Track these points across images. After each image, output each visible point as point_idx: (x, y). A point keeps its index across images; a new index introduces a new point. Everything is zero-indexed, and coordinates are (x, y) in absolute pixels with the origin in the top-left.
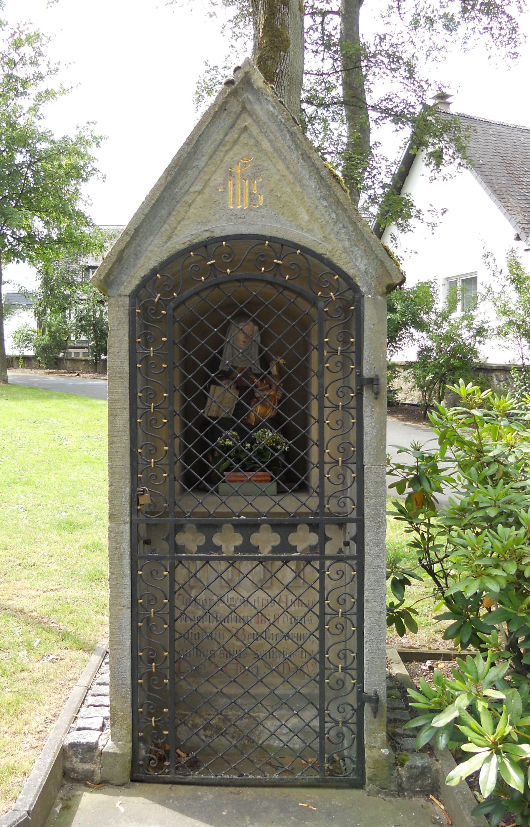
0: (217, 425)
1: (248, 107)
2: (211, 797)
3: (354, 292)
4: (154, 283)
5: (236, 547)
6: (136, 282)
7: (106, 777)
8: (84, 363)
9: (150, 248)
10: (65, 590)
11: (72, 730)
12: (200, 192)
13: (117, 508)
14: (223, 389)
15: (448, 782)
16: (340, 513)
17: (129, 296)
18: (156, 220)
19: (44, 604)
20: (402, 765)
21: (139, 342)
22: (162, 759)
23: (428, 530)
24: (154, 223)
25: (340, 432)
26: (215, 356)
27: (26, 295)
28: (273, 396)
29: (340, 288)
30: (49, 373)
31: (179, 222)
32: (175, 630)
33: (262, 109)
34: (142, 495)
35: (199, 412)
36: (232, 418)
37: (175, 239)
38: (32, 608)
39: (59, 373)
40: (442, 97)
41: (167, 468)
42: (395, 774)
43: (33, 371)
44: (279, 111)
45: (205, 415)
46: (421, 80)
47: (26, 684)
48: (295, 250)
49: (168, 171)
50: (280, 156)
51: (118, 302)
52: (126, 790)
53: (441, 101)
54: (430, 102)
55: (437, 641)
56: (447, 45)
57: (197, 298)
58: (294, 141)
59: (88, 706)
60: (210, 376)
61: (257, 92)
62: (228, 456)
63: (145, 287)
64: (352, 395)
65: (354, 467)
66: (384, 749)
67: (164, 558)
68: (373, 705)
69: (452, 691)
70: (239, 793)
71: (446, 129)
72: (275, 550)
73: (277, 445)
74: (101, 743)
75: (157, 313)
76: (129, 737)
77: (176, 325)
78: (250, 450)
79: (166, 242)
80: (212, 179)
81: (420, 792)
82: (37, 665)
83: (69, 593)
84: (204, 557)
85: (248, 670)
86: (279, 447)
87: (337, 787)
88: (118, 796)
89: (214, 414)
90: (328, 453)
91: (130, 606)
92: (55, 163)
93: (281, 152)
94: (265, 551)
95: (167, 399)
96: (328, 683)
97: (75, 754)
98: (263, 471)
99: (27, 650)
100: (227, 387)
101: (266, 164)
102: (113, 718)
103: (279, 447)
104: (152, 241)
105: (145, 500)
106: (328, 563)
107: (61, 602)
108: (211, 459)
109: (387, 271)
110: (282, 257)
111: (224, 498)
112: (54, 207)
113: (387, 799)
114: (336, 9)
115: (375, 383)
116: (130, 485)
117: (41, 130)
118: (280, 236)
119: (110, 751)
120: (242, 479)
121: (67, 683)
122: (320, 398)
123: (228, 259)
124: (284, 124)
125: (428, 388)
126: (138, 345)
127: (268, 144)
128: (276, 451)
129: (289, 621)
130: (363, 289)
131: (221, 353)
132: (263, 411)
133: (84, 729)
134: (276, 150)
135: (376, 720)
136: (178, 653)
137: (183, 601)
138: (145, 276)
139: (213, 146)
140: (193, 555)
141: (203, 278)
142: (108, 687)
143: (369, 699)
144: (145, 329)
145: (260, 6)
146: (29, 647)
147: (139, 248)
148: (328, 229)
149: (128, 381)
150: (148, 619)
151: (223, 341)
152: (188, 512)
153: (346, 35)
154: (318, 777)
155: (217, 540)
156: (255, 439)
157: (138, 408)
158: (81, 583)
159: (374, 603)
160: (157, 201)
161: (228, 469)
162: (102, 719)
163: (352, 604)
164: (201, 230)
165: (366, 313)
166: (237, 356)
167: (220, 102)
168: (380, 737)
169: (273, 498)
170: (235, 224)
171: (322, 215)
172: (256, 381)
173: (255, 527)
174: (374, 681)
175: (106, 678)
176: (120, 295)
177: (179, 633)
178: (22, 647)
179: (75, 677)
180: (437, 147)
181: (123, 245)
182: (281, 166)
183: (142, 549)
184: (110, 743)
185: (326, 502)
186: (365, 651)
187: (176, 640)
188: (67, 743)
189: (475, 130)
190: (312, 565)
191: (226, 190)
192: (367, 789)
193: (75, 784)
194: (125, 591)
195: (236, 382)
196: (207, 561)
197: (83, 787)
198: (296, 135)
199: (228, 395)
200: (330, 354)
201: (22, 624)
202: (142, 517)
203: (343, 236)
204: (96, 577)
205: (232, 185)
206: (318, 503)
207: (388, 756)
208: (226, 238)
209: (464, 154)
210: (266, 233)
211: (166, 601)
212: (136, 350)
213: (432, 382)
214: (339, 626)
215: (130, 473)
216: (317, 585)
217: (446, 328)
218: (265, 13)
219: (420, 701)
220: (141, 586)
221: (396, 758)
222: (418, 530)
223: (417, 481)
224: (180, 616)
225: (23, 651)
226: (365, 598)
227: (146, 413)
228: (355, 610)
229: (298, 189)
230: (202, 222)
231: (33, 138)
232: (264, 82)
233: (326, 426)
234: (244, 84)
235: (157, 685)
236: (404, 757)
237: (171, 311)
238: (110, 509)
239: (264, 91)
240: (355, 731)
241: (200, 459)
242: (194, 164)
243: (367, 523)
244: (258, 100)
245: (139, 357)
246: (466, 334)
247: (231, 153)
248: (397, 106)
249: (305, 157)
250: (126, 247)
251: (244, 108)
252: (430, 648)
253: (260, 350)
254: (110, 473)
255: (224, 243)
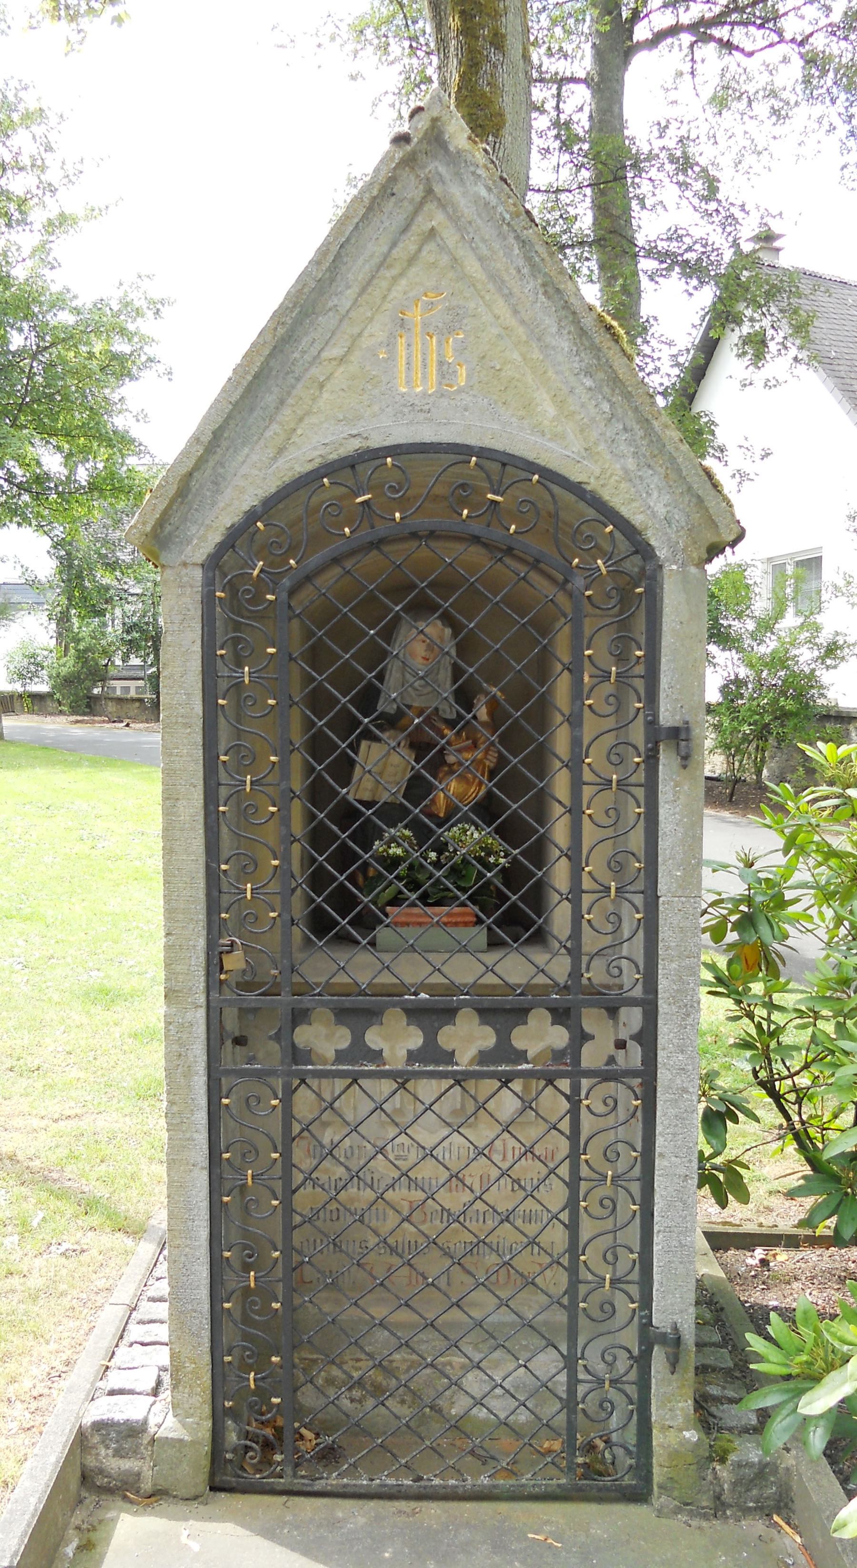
0: (374, 818)
1: (438, 189)
2: (361, 1520)
3: (644, 559)
4: (252, 540)
5: (410, 1052)
6: (216, 537)
7: (163, 1484)
8: (137, 704)
9: (244, 470)
10: (93, 1117)
11: (98, 1394)
12: (342, 360)
13: (181, 978)
14: (386, 747)
15: (835, 1531)
16: (608, 987)
17: (203, 565)
18: (255, 414)
19: (53, 1144)
20: (723, 1460)
21: (222, 656)
22: (268, 1446)
23: (769, 1016)
24: (251, 420)
25: (610, 832)
26: (370, 685)
27: (33, 584)
28: (481, 762)
29: (616, 551)
30: (77, 722)
31: (301, 420)
32: (293, 1210)
33: (465, 194)
34: (228, 952)
35: (338, 793)
36: (401, 804)
37: (292, 453)
38: (31, 1152)
39: (94, 722)
40: (767, 238)
41: (277, 901)
42: (710, 1477)
43: (49, 719)
44: (499, 198)
45: (350, 798)
46: (732, 204)
47: (16, 1300)
48: (529, 475)
49: (278, 317)
50: (500, 290)
51: (181, 578)
52: (201, 1507)
53: (764, 245)
54: (747, 247)
55: (771, 1210)
56: (774, 146)
57: (337, 571)
58: (529, 259)
59: (131, 1345)
60: (360, 723)
61: (455, 159)
62: (395, 878)
63: (233, 546)
64: (637, 760)
65: (638, 900)
66: (688, 1430)
67: (272, 1073)
68: (669, 1350)
69: (837, 1344)
70: (414, 1513)
71: (772, 294)
72: (484, 1057)
73: (489, 854)
74: (152, 1422)
75: (258, 598)
76: (207, 1409)
77: (295, 623)
78: (437, 865)
79: (275, 459)
80: (366, 334)
81: (755, 1509)
82: (39, 1262)
83: (100, 1123)
84: (348, 1071)
85: (433, 1284)
86: (492, 860)
87: (600, 1500)
88: (186, 1519)
89: (366, 796)
90: (590, 873)
91: (206, 1164)
92: (84, 349)
93: (503, 282)
94: (465, 1060)
95: (276, 766)
96: (584, 1309)
97: (103, 1442)
98: (463, 905)
99: (21, 1234)
100: (393, 744)
101: (472, 305)
102: (176, 1368)
103: (492, 860)
104: (247, 456)
105: (235, 962)
106: (585, 1083)
107: (84, 1140)
108: (360, 880)
109: (710, 517)
110: (502, 489)
111: (387, 958)
112: (82, 427)
113: (694, 1523)
114: (582, 75)
115: (683, 736)
116: (205, 932)
117: (55, 288)
118: (498, 446)
119: (171, 1435)
120: (421, 920)
121: (93, 1297)
122: (575, 765)
123: (398, 492)
124: (508, 224)
125: (738, 750)
126: (219, 661)
127: (477, 265)
128: (489, 867)
129: (510, 1188)
130: (662, 553)
131: (381, 677)
132: (461, 790)
133: (121, 1392)
134: (493, 277)
135: (675, 1376)
136: (299, 1253)
137: (309, 1151)
138: (232, 526)
139: (367, 267)
140: (329, 1067)
141: (347, 530)
142: (167, 1304)
143: (663, 1339)
144: (235, 631)
145: (452, 49)
146: (25, 1228)
147: (221, 470)
148: (594, 435)
149: (201, 732)
150: (243, 1188)
151: (384, 654)
152: (318, 985)
153: (600, 122)
154: (563, 1481)
155: (373, 1038)
156: (446, 844)
157: (219, 784)
158: (121, 1104)
159: (673, 1159)
160: (256, 377)
161: (396, 901)
162: (157, 1369)
163: (632, 1161)
164: (345, 435)
165: (666, 601)
166: (411, 686)
167: (382, 179)
168: (682, 1409)
169: (480, 956)
170: (411, 423)
171: (583, 406)
172: (449, 733)
173: (449, 1014)
174: (672, 1305)
175: (163, 1288)
176: (185, 564)
177: (301, 1215)
178: (10, 1228)
179: (107, 1286)
180: (757, 326)
181: (190, 464)
182: (502, 308)
183: (229, 1054)
184: (171, 1421)
185: (584, 966)
186: (655, 1248)
187: (295, 1227)
188: (88, 1421)
189: (827, 291)
190: (555, 1087)
191: (392, 356)
192: (656, 1503)
193: (103, 1497)
194: (196, 1136)
195: (409, 735)
196: (355, 1079)
197: (120, 1503)
198: (532, 245)
199: (395, 759)
200: (596, 680)
201: (11, 1182)
202: (228, 995)
203: (623, 447)
204: (151, 1092)
205: (405, 345)
206: (569, 969)
207: (697, 1444)
208: (395, 450)
209: (807, 337)
210: (472, 440)
211: (275, 1155)
212: (216, 671)
213: (746, 739)
214: (606, 1202)
215: (204, 911)
216: (565, 1125)
217: (768, 647)
218: (460, 63)
219: (771, 1358)
220: (227, 1126)
221: (711, 1446)
222: (750, 1016)
223: (747, 922)
224: (303, 1184)
225: (11, 1234)
226: (658, 1150)
227: (238, 793)
228: (637, 1171)
229: (536, 355)
230: (345, 418)
231: (41, 304)
232: (470, 138)
233: (585, 820)
234: (429, 143)
235: (257, 1313)
236: (726, 1445)
237: (284, 595)
238: (167, 980)
239: (469, 158)
240: (635, 1396)
241: (342, 884)
242: (330, 304)
243: (663, 1007)
244: (457, 174)
245: (223, 685)
246: (805, 656)
247: (403, 282)
248: (690, 249)
249: (551, 290)
250: (197, 467)
251: (429, 191)
252: (761, 1225)
253: (457, 672)
254: (166, 910)
255: (389, 460)
